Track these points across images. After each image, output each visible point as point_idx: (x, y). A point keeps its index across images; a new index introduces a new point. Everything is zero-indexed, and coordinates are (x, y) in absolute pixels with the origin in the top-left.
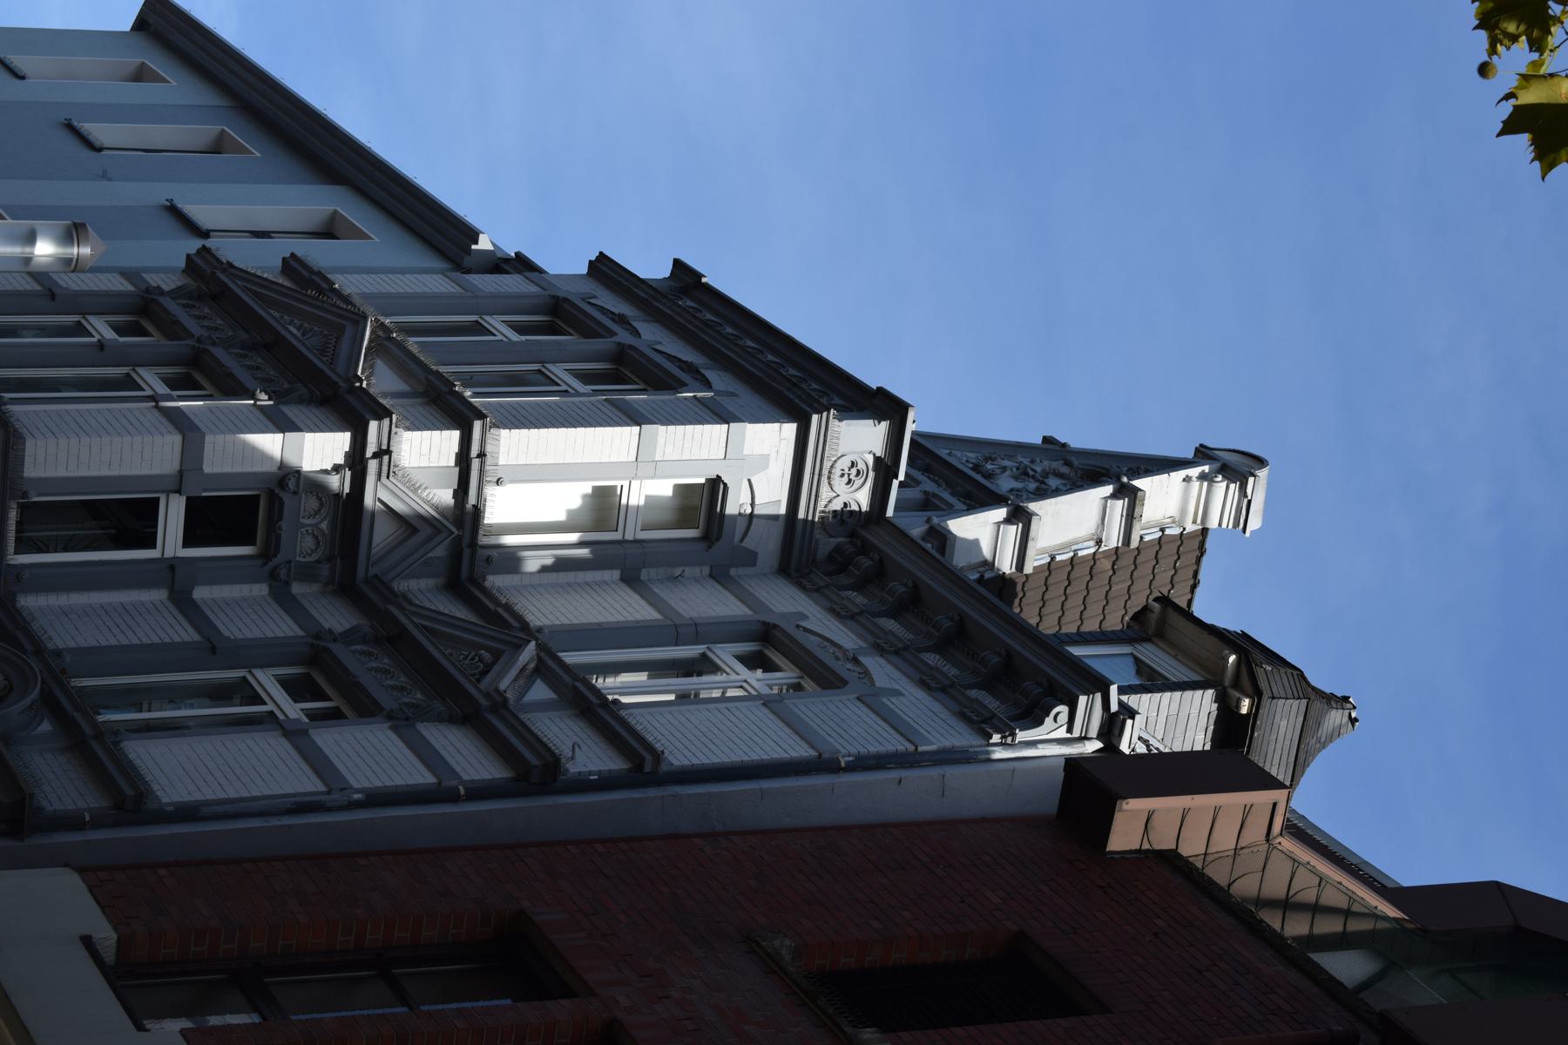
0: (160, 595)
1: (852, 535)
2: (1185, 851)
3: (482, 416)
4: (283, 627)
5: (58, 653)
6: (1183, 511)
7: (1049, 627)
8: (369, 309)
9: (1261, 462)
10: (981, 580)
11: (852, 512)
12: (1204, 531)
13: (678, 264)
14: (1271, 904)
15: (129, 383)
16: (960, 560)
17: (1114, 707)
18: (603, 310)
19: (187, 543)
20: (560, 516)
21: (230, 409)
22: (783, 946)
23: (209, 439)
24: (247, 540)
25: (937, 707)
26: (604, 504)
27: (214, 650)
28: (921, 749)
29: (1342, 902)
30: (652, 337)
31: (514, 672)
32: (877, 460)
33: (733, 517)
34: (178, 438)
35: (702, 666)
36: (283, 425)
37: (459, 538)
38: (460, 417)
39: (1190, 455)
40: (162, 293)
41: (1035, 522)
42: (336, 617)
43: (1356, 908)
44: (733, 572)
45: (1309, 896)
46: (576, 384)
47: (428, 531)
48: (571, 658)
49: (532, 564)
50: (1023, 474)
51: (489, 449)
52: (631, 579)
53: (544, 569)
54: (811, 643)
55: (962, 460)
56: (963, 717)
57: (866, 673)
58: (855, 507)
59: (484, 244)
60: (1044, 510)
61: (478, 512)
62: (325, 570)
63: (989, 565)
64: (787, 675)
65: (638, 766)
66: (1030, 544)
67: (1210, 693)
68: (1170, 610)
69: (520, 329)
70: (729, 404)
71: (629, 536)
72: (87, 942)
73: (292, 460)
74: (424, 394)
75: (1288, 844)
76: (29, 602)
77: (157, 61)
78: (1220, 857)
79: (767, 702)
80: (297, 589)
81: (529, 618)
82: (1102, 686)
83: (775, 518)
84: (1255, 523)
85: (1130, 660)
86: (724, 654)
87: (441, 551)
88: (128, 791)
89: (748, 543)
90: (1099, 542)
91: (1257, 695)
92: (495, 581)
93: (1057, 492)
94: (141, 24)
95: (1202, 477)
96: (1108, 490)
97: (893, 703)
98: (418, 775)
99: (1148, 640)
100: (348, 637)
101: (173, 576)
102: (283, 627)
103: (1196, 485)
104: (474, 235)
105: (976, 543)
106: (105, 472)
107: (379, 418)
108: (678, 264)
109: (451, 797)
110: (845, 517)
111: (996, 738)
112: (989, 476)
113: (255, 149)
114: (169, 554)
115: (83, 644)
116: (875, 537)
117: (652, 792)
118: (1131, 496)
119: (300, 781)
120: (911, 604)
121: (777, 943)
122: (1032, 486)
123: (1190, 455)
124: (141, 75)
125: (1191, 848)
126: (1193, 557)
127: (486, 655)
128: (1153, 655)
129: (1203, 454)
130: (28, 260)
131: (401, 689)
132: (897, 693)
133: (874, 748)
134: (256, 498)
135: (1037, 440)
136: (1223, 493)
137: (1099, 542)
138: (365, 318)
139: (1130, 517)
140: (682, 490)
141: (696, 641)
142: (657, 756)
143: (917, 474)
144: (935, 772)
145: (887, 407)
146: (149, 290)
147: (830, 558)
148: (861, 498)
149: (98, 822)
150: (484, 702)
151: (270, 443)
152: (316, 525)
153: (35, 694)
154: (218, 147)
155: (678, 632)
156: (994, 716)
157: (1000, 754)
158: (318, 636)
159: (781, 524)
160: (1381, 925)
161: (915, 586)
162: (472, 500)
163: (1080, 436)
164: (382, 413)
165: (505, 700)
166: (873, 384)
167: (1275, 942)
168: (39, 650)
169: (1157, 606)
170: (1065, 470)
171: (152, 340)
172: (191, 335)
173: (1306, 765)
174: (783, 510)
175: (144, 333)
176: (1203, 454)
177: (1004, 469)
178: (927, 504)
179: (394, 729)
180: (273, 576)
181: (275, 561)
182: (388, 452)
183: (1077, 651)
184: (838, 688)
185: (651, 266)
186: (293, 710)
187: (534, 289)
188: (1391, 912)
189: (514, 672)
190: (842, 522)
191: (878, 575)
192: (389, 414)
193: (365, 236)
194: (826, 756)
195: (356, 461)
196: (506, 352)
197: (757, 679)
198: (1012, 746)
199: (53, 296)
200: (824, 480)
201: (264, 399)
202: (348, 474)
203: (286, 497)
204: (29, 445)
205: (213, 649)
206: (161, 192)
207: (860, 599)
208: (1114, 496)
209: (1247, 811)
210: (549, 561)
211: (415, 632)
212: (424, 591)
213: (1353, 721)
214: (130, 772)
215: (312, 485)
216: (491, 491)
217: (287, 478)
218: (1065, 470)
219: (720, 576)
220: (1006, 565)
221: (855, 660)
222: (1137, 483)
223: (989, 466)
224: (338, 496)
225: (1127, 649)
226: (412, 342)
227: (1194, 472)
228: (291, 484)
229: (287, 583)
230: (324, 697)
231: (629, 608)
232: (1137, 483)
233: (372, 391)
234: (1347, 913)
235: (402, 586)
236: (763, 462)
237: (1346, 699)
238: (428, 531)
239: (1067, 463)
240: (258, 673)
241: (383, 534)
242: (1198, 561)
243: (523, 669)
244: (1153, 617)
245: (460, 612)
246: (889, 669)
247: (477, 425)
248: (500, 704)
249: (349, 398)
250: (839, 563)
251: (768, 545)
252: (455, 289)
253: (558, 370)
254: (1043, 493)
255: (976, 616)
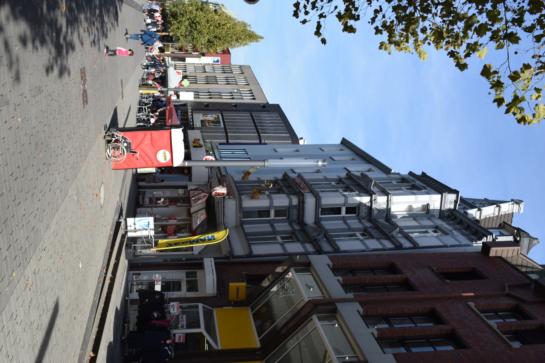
0: (342, 222)
1: (451, 212)
2: (503, 256)
3: (390, 194)
4: (360, 226)
5: (327, 230)
6: (509, 210)
7: (486, 227)
8: (373, 180)
9: (522, 201)
10: (473, 220)
11: (451, 209)
12: (513, 213)
13: (423, 173)
14: (519, 266)
15: (337, 191)
16: (469, 217)
17: (494, 238)
18: (410, 179)
19: (346, 214)
20: (404, 210)
21: (352, 194)
22: (435, 268)
23: (349, 198)
24: (355, 213)
25: (464, 238)
26: (410, 208)
27: (350, 229)
28: (462, 244)
29: (532, 266)
30: (418, 183)
31: (395, 232)
32: (455, 200)
33: (431, 210)
34: (344, 198)
35: (426, 232)
36: (360, 196)
37: (387, 213)
38: (387, 194)
39: (510, 201)
40: (342, 178)
41: (482, 211)
42: (368, 225)
43: (534, 267)
44: (431, 218)
45: (526, 265)
46: (406, 190)
47: (382, 212)
48: (405, 231)
49: (399, 217)
50: (481, 204)
51: (391, 199)
52: (415, 219)
53: (401, 218)
54: (444, 229)
55: (470, 202)
56: (469, 239)
57: (453, 233)
58: (451, 208)
59: (393, 171)
60: (484, 209)
61: (390, 209)
62: (367, 218)
63: (475, 218)
64: (440, 233)
65: (415, 246)
66: (482, 214)
67: (512, 237)
68: (506, 225)
69: (397, 182)
70: (430, 192)
71: (414, 213)
72: (328, 265)
73: (361, 201)
74: (382, 191)
75: (521, 256)
76: (323, 223)
77: (344, 148)
78: (509, 258)
79: (436, 237)
80: (363, 221)
81: (398, 224)
82: (492, 234)
83: (438, 210)
84: (522, 211)
85: (499, 232)
86: (430, 230)
87: (384, 215)
88: (336, 248)
89: (434, 214)
90: (494, 214)
91: (520, 237)
92: (393, 220)
93: (486, 206)
94: (342, 143)
95: (512, 204)
96: (495, 206)
97: (457, 237)
98: (380, 247)
99: (501, 229)
100: (370, 227)
101: (344, 219)
102: (360, 226)
103: (511, 205)
104: (391, 170)
105: (472, 214)
106: (333, 203)
107: (374, 194)
108: (423, 173)
109: (385, 250)
110: (449, 210)
111: (474, 242)
112: (475, 204)
113: (358, 159)
114: (343, 215)
115: (330, 228)
116: (454, 212)
117: (417, 250)
118: (499, 207)
119: (362, 247)
120: (461, 222)
121: (434, 268)
122: (482, 205)
123: (510, 201)
124: (341, 150)
125: (504, 256)
126: (511, 217)
127: (391, 230)
128: (502, 231)
129: (512, 200)
130: (317, 165)
131: (376, 232)
132: (458, 236)
133: (453, 244)
134: (356, 207)
135: (483, 199)
136: (516, 206)
137: (494, 214)
138: (373, 181)
139: (499, 210)
140: (423, 206)
141: (425, 228)
142: (418, 244)
143: (461, 203)
144: (464, 248)
145: (456, 192)
146: (340, 178)
147: (447, 216)
148: (452, 207)
149: (332, 253)
150: (391, 236)
151: (358, 199)
152: (365, 211)
153: (323, 234)
154: (353, 159)
155: (422, 227)
156: (474, 239)
157: (475, 245)
158: (366, 227)
159: (439, 211)
160: (539, 270)
161: (456, 216)
162: (389, 207)
163: (490, 198)
164: (375, 194)
165: (394, 236)
166: (454, 189)
167: (519, 271)
168: (324, 229)
169: (503, 223)
170: (488, 203)
171: (341, 185)
172: (346, 184)
173: (530, 249)
174: (439, 208)
175: (340, 184)
176: (512, 200)
177: (477, 203)
178: (464, 208)
179: (377, 240)
180: (359, 219)
181: (359, 216)
182: (376, 200)
183: (490, 230)
184: (447, 235)
185: (419, 173)
186: (361, 238)
187: (400, 177)
188: (541, 268)
189: (395, 232)
190: (449, 210)
191: (455, 218)
192: (376, 194)
193: (374, 171)
194: (445, 245)
195: (371, 201)
196: (395, 186)
197: (435, 234)
198: (477, 244)
199: (326, 179)
200: (446, 203)
201: (357, 192)
202: (370, 203)
203: (360, 207)
204: (322, 199)
205: (350, 229)
206: (344, 166)
207: (452, 222)
208: (496, 207)
209: (514, 250)
210: (402, 217)
211: (380, 227)
212: (382, 221)
213: (539, 242)
214: (337, 245)
215: (365, 205)
216: (392, 206)
217: (360, 204)
218: (488, 203)
219: (429, 219)
220: (478, 218)
221: (451, 231)
222: (500, 205)
223: (475, 203)
224: (368, 206)
225: (498, 230)
226: (380, 185)
227: (511, 203)
228: (361, 205)
229: (361, 220)
230: (366, 236)
231: (415, 223)
232: (500, 205)
233: (374, 191)
234: (533, 268)
235: (378, 220)
236: (436, 201)
237: (537, 238)
238: (382, 212)
239: (488, 202)
240: (357, 233)
241: (375, 212)
242: (512, 218)
243: (397, 232)
244: (502, 225)
245: (387, 224)
246: (457, 232)
247: (390, 195)
248: (393, 237)
249: (370, 192)
250: (449, 217)
251: (437, 214)
252: (387, 177)
253: (403, 188)
254: (484, 206)
255: (471, 224)
